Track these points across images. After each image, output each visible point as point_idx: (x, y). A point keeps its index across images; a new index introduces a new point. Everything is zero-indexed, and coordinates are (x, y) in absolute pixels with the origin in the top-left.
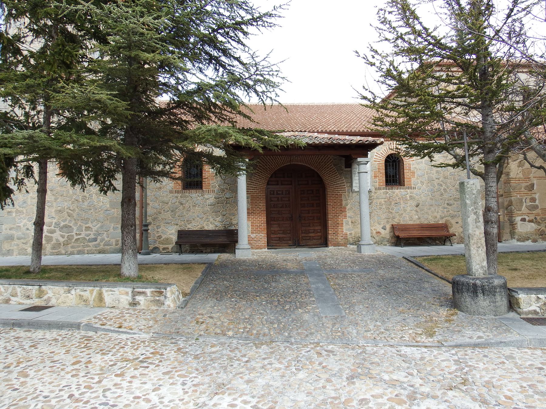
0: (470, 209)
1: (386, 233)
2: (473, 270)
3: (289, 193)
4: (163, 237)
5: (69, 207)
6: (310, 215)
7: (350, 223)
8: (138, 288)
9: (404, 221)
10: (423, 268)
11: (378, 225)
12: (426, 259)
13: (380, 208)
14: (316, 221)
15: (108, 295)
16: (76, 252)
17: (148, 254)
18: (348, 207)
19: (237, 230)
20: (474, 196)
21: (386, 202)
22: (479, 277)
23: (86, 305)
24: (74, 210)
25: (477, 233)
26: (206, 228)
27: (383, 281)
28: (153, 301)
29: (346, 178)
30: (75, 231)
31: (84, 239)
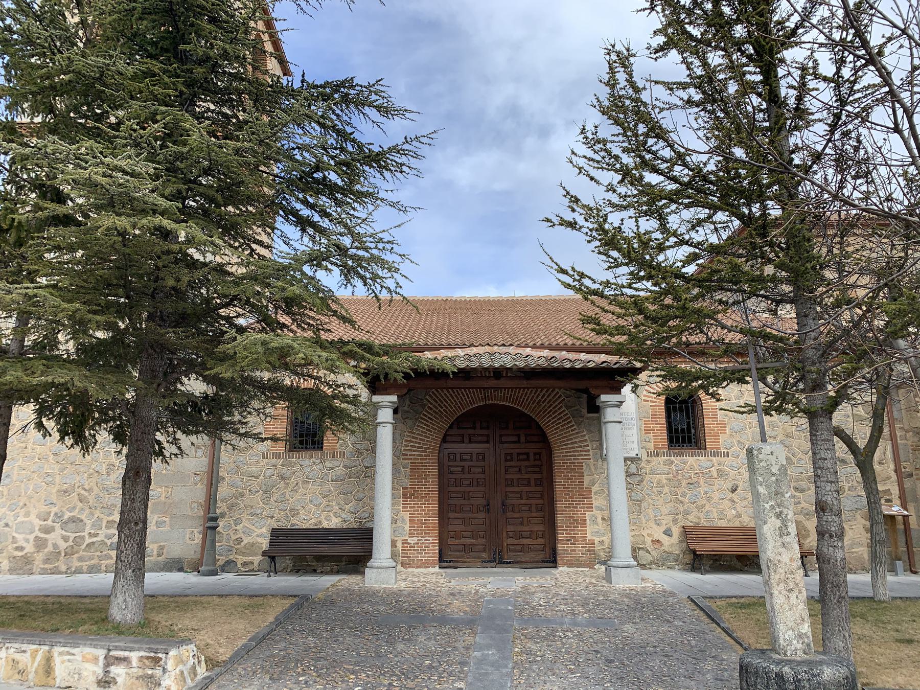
0: (767, 506)
1: (672, 543)
2: (781, 642)
3: (484, 458)
4: (245, 541)
5: (83, 485)
6: (523, 501)
7: (599, 520)
8: (117, 648)
9: (708, 520)
10: (718, 625)
11: (655, 527)
12: (731, 605)
13: (660, 493)
14: (534, 515)
15: (63, 662)
16: (85, 568)
17: (214, 573)
18: (594, 489)
19: (372, 529)
20: (774, 478)
21: (669, 480)
22: (794, 657)
23: (22, 682)
24: (90, 490)
25: (785, 558)
26: (325, 525)
27: (623, 649)
28: (141, 676)
29: (590, 432)
30: (88, 529)
31: (103, 543)
